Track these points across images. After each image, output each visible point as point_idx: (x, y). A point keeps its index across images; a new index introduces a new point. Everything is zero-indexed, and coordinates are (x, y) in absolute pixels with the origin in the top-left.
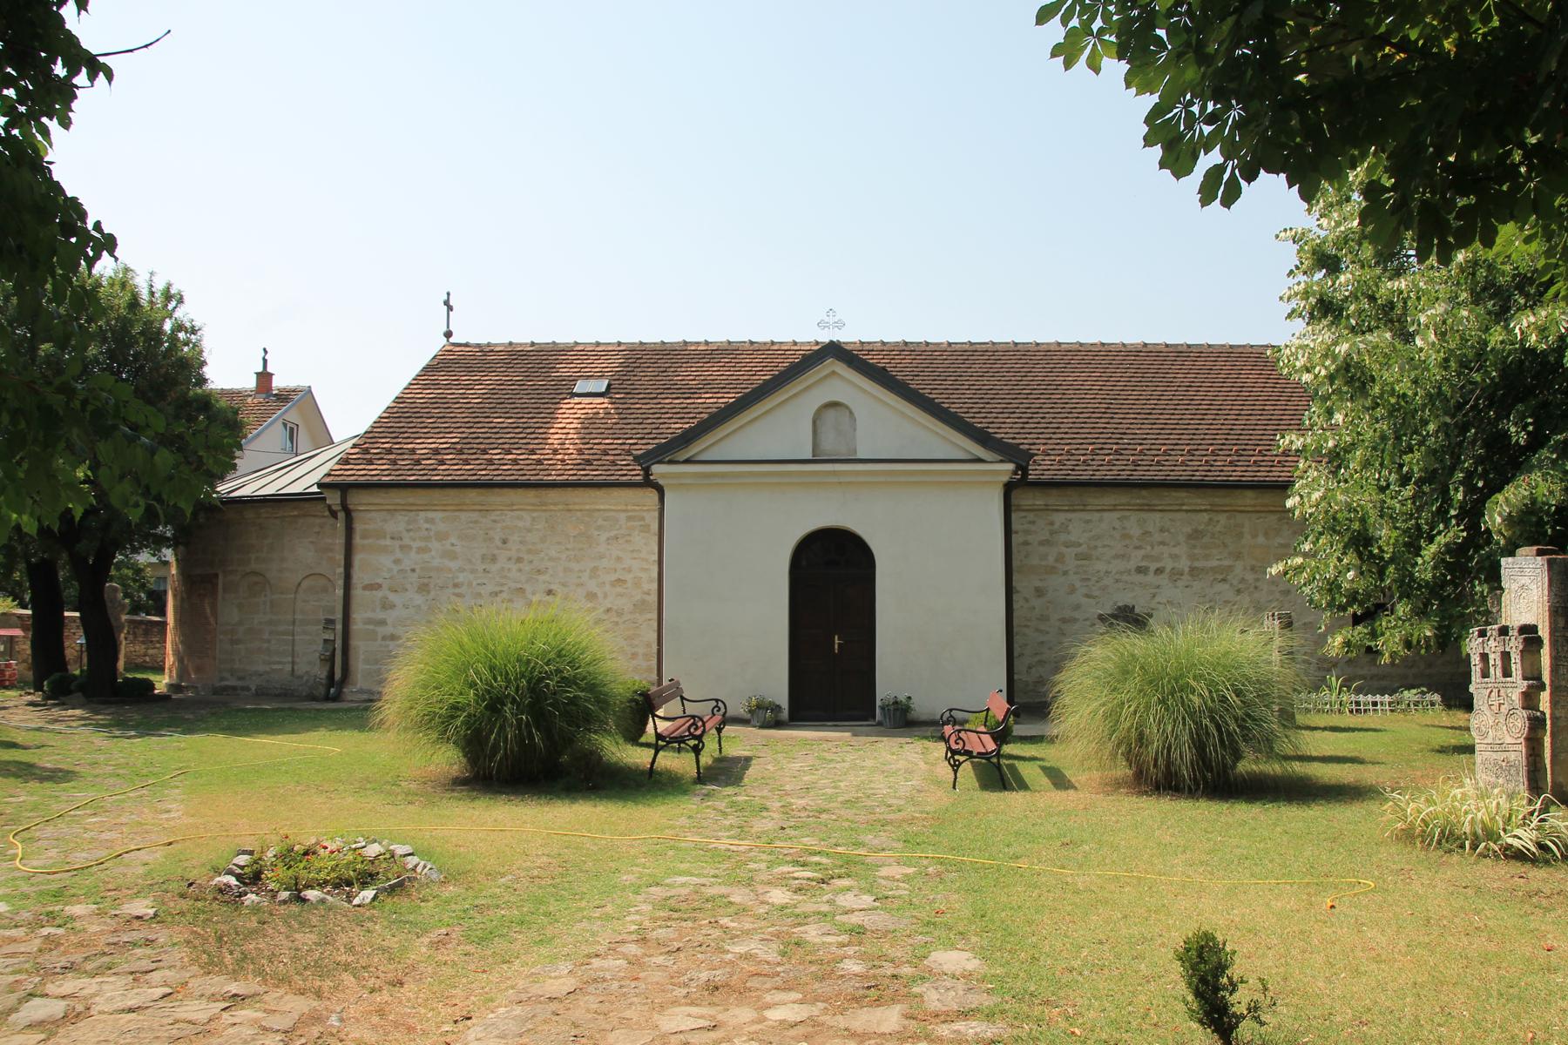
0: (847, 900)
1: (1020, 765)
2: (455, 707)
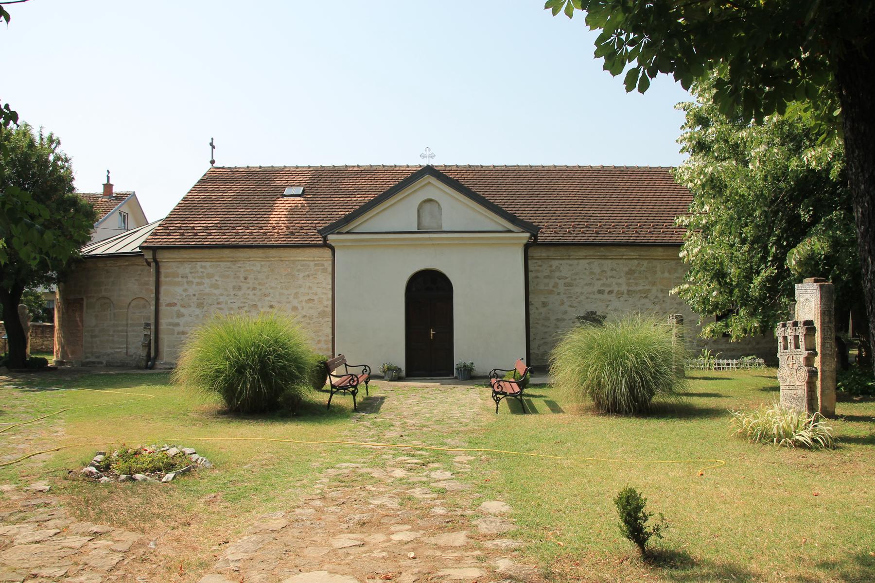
0: (436, 475)
2: (218, 371)
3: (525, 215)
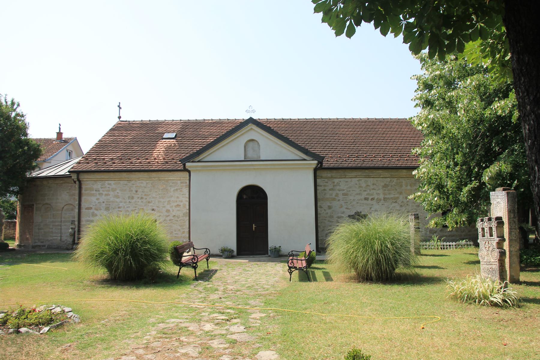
0: (234, 329)
1: (316, 272)
3: (317, 150)
